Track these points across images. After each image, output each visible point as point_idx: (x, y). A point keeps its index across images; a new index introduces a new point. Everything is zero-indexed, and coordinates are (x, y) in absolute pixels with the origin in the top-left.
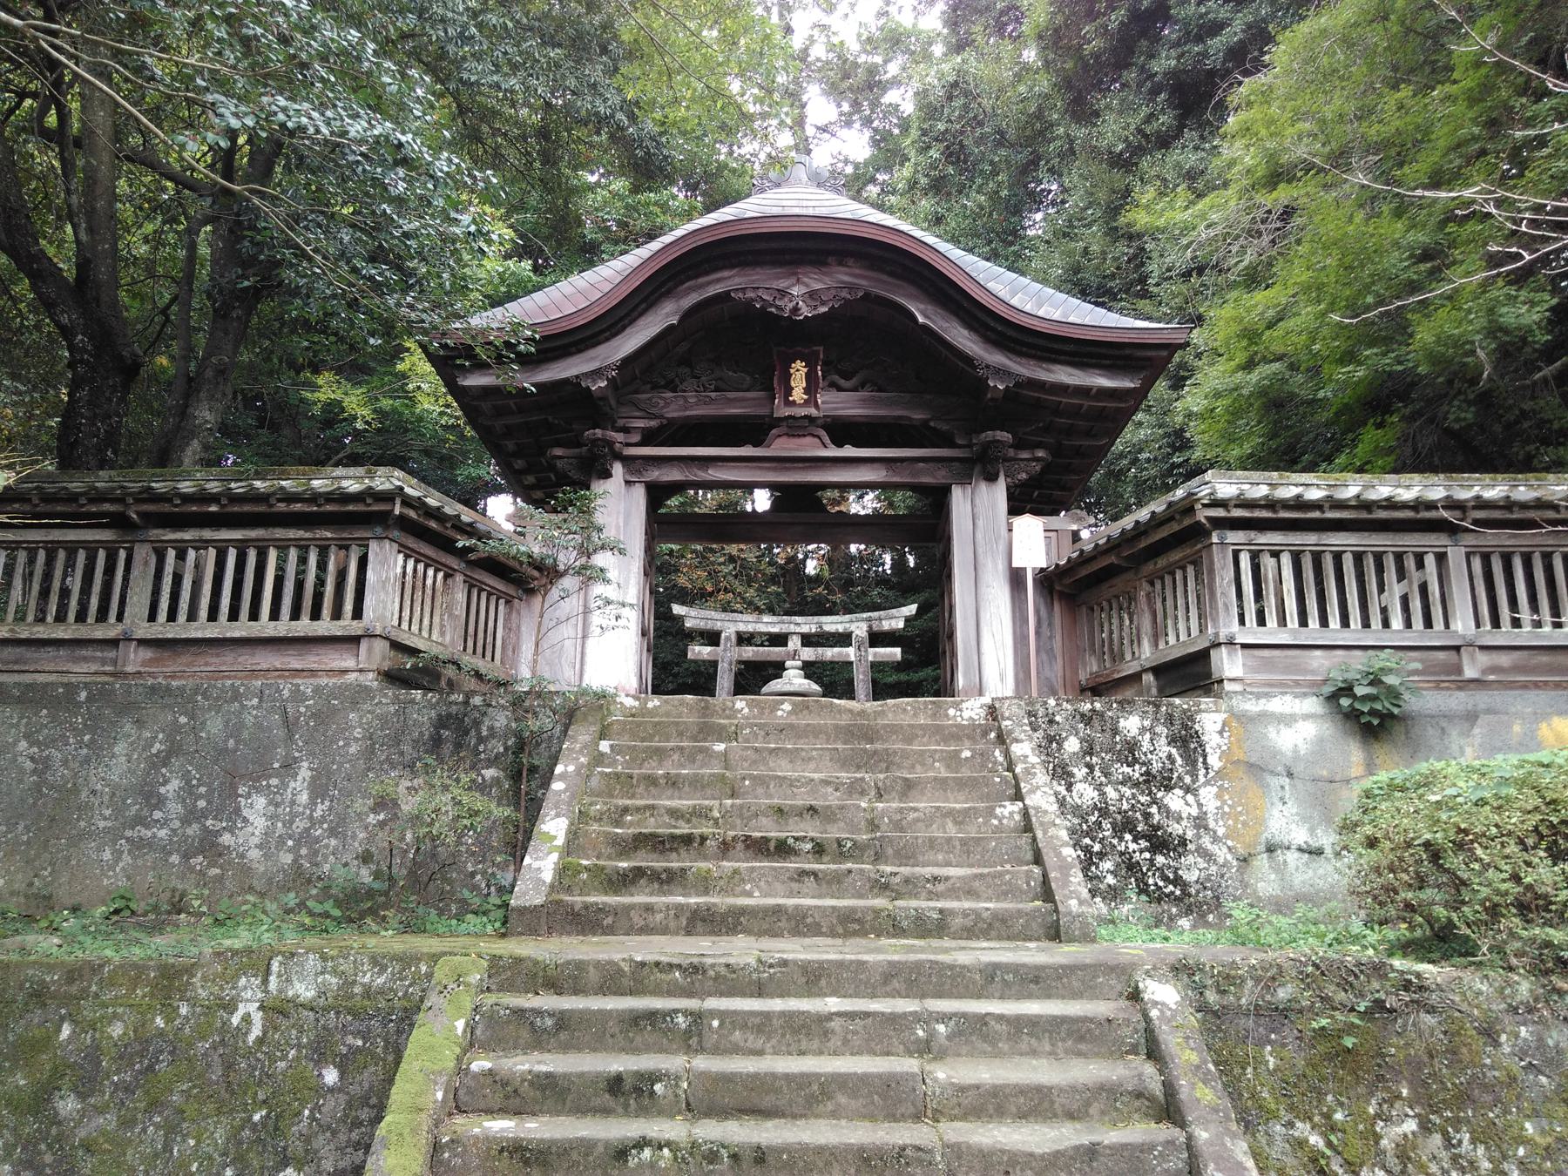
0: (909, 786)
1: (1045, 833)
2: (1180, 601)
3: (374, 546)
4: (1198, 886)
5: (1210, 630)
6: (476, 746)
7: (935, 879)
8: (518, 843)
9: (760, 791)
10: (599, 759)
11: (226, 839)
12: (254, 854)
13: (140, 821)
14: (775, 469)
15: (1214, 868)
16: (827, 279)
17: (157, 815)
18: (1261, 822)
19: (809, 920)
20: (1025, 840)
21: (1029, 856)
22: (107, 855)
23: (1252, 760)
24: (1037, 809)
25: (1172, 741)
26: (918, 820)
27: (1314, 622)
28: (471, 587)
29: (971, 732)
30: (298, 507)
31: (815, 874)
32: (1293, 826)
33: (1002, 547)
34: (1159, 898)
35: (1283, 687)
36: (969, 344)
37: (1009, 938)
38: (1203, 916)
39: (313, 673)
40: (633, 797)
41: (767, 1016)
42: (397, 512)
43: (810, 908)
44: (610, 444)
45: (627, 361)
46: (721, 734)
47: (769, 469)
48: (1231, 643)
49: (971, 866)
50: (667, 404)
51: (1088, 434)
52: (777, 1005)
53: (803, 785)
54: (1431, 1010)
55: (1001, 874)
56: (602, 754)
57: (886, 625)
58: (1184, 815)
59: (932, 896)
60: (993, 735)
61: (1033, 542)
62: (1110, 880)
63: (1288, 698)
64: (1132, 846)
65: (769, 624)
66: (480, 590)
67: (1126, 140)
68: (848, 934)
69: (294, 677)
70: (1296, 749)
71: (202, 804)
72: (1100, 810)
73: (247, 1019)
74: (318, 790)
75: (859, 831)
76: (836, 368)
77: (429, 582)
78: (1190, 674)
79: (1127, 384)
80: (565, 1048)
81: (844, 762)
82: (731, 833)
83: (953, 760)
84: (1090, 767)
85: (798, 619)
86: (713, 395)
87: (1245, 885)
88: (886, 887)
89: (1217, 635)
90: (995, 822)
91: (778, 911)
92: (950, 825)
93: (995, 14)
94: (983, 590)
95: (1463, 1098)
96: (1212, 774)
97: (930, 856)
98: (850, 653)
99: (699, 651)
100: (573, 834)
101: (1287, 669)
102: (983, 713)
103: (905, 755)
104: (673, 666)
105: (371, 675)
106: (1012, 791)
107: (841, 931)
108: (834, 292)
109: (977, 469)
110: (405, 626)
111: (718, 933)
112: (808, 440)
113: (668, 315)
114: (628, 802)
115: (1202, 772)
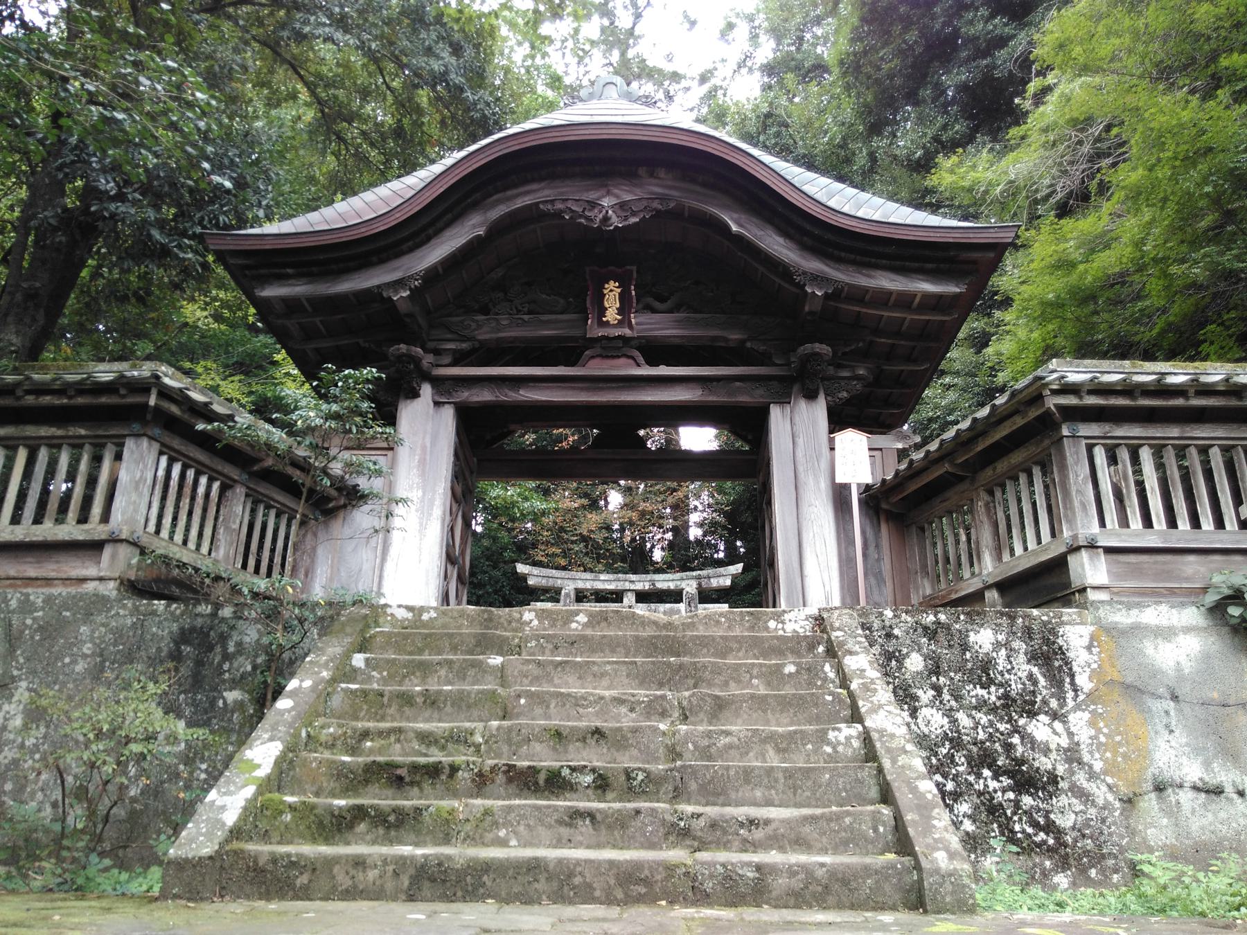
1: (894, 761)
2: (1027, 507)
3: (130, 444)
4: (1075, 834)
5: (1066, 533)
6: (220, 665)
7: (751, 822)
9: (538, 711)
10: (345, 672)
14: (587, 389)
15: (1092, 812)
16: (638, 191)
18: (1145, 754)
19: (577, 880)
20: (868, 770)
21: (874, 792)
23: (1129, 680)
24: (881, 732)
25: (1033, 658)
26: (730, 747)
27: (1184, 524)
28: (256, 503)
29: (796, 646)
30: (47, 400)
31: (591, 815)
32: (1184, 760)
33: (824, 464)
34: (1028, 848)
35: (1156, 595)
36: (785, 251)
37: (852, 907)
38: (1083, 871)
39: (48, 581)
40: (383, 719)
42: (152, 402)
43: (578, 862)
44: (417, 361)
45: (433, 276)
46: (501, 647)
47: (582, 389)
49: (798, 805)
50: (479, 327)
51: (909, 359)
53: (591, 704)
55: (838, 817)
56: (355, 670)
57: (714, 583)
58: (1053, 746)
59: (748, 845)
60: (821, 649)
61: (857, 458)
63: (1164, 608)
64: (993, 785)
66: (268, 507)
67: (924, 147)
68: (631, 900)
69: (26, 586)
72: (951, 740)
75: (656, 760)
77: (201, 490)
78: (1047, 584)
79: (952, 289)
81: (644, 679)
82: (491, 762)
83: (774, 676)
84: (938, 689)
85: (633, 577)
86: (526, 317)
87: (1132, 833)
88: (685, 833)
89: (1075, 537)
90: (828, 749)
91: (534, 867)
92: (771, 752)
94: (805, 509)
96: (1082, 697)
97: (745, 792)
101: (1158, 576)
102: (808, 625)
103: (717, 670)
105: (112, 585)
106: (847, 712)
107: (620, 895)
108: (645, 203)
109: (796, 388)
110: (165, 534)
111: (451, 899)
112: (622, 361)
113: (474, 226)
114: (371, 725)
115: (1070, 695)
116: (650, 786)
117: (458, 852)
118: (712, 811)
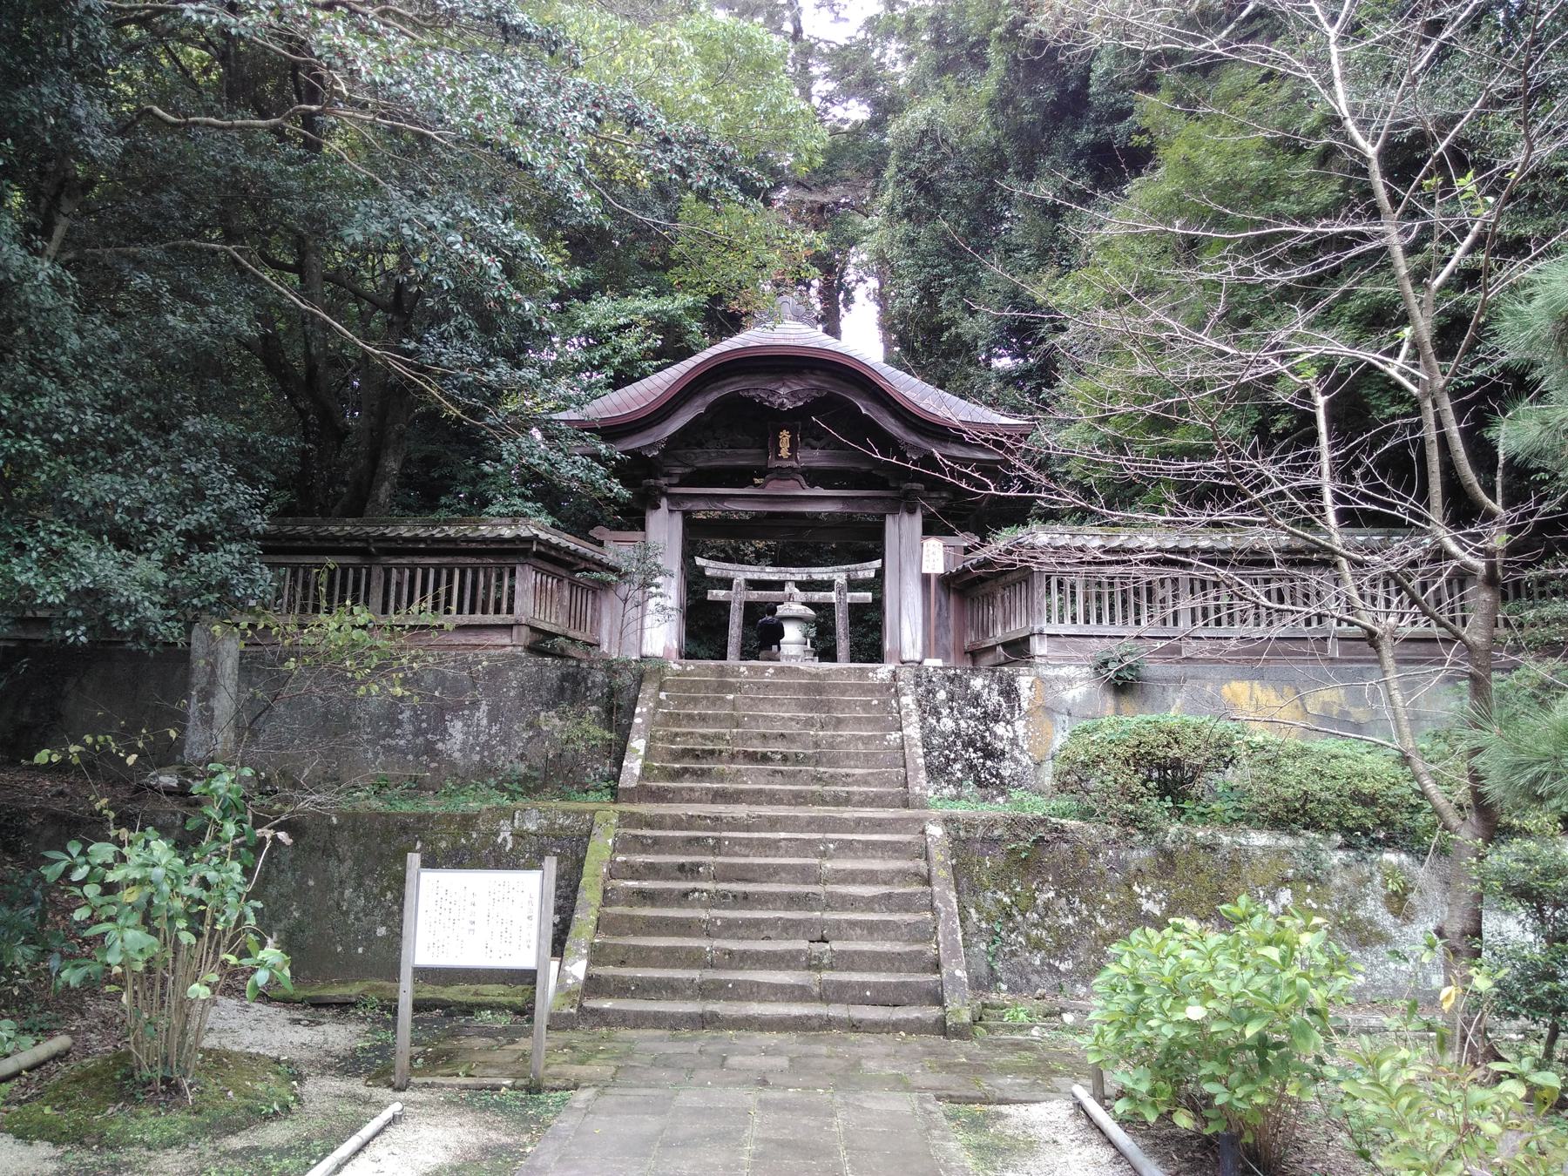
0: (839, 721)
3: (519, 568)
8: (618, 753)
10: (659, 703)
11: (440, 746)
12: (457, 755)
13: (388, 735)
17: (398, 731)
22: (370, 755)
25: (1001, 693)
27: (1093, 621)
41: (751, 839)
44: (659, 488)
46: (731, 688)
48: (1041, 634)
52: (756, 835)
54: (1067, 842)
57: (861, 575)
61: (935, 556)
62: (959, 775)
65: (770, 573)
70: (1074, 699)
71: (424, 725)
73: (505, 839)
74: (493, 717)
76: (806, 435)
80: (657, 853)
81: (804, 706)
83: (867, 706)
84: (952, 709)
85: (793, 570)
87: (1037, 778)
88: (820, 779)
91: (760, 792)
93: (966, 45)
95: (1077, 882)
97: (847, 762)
98: (833, 596)
99: (717, 594)
100: (648, 749)
104: (703, 627)
116: (806, 760)
117: (728, 786)
118: (831, 770)
